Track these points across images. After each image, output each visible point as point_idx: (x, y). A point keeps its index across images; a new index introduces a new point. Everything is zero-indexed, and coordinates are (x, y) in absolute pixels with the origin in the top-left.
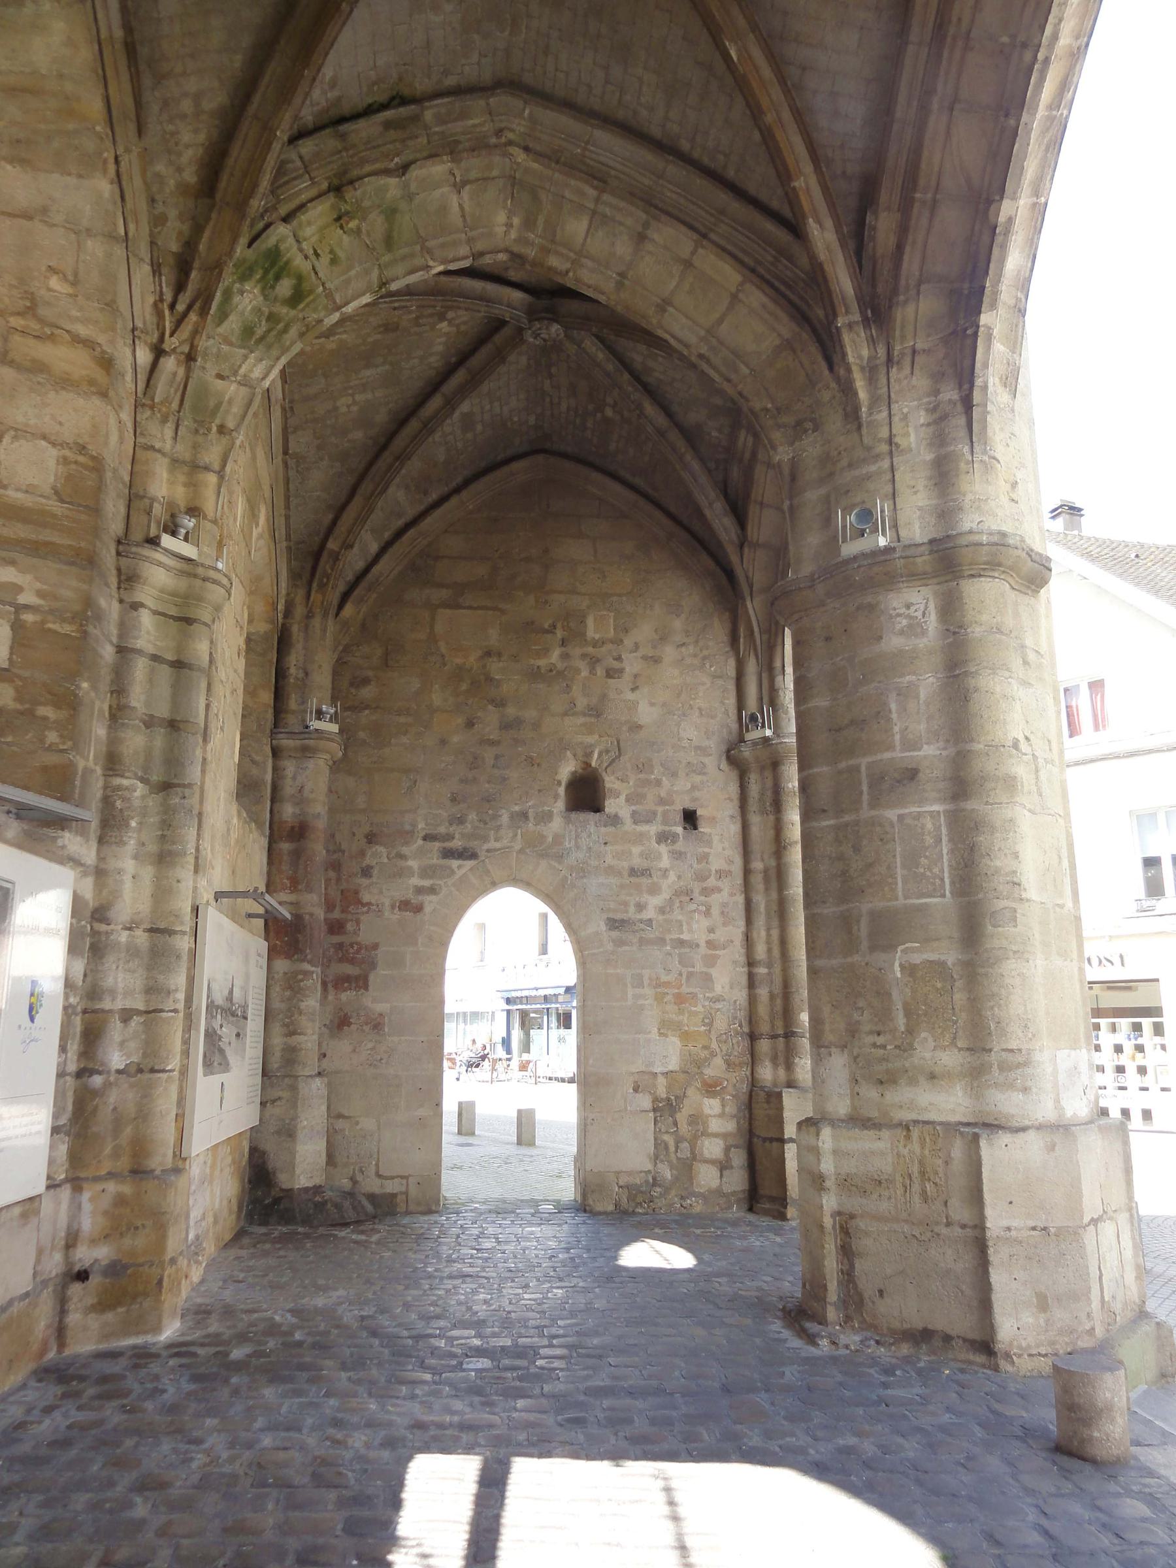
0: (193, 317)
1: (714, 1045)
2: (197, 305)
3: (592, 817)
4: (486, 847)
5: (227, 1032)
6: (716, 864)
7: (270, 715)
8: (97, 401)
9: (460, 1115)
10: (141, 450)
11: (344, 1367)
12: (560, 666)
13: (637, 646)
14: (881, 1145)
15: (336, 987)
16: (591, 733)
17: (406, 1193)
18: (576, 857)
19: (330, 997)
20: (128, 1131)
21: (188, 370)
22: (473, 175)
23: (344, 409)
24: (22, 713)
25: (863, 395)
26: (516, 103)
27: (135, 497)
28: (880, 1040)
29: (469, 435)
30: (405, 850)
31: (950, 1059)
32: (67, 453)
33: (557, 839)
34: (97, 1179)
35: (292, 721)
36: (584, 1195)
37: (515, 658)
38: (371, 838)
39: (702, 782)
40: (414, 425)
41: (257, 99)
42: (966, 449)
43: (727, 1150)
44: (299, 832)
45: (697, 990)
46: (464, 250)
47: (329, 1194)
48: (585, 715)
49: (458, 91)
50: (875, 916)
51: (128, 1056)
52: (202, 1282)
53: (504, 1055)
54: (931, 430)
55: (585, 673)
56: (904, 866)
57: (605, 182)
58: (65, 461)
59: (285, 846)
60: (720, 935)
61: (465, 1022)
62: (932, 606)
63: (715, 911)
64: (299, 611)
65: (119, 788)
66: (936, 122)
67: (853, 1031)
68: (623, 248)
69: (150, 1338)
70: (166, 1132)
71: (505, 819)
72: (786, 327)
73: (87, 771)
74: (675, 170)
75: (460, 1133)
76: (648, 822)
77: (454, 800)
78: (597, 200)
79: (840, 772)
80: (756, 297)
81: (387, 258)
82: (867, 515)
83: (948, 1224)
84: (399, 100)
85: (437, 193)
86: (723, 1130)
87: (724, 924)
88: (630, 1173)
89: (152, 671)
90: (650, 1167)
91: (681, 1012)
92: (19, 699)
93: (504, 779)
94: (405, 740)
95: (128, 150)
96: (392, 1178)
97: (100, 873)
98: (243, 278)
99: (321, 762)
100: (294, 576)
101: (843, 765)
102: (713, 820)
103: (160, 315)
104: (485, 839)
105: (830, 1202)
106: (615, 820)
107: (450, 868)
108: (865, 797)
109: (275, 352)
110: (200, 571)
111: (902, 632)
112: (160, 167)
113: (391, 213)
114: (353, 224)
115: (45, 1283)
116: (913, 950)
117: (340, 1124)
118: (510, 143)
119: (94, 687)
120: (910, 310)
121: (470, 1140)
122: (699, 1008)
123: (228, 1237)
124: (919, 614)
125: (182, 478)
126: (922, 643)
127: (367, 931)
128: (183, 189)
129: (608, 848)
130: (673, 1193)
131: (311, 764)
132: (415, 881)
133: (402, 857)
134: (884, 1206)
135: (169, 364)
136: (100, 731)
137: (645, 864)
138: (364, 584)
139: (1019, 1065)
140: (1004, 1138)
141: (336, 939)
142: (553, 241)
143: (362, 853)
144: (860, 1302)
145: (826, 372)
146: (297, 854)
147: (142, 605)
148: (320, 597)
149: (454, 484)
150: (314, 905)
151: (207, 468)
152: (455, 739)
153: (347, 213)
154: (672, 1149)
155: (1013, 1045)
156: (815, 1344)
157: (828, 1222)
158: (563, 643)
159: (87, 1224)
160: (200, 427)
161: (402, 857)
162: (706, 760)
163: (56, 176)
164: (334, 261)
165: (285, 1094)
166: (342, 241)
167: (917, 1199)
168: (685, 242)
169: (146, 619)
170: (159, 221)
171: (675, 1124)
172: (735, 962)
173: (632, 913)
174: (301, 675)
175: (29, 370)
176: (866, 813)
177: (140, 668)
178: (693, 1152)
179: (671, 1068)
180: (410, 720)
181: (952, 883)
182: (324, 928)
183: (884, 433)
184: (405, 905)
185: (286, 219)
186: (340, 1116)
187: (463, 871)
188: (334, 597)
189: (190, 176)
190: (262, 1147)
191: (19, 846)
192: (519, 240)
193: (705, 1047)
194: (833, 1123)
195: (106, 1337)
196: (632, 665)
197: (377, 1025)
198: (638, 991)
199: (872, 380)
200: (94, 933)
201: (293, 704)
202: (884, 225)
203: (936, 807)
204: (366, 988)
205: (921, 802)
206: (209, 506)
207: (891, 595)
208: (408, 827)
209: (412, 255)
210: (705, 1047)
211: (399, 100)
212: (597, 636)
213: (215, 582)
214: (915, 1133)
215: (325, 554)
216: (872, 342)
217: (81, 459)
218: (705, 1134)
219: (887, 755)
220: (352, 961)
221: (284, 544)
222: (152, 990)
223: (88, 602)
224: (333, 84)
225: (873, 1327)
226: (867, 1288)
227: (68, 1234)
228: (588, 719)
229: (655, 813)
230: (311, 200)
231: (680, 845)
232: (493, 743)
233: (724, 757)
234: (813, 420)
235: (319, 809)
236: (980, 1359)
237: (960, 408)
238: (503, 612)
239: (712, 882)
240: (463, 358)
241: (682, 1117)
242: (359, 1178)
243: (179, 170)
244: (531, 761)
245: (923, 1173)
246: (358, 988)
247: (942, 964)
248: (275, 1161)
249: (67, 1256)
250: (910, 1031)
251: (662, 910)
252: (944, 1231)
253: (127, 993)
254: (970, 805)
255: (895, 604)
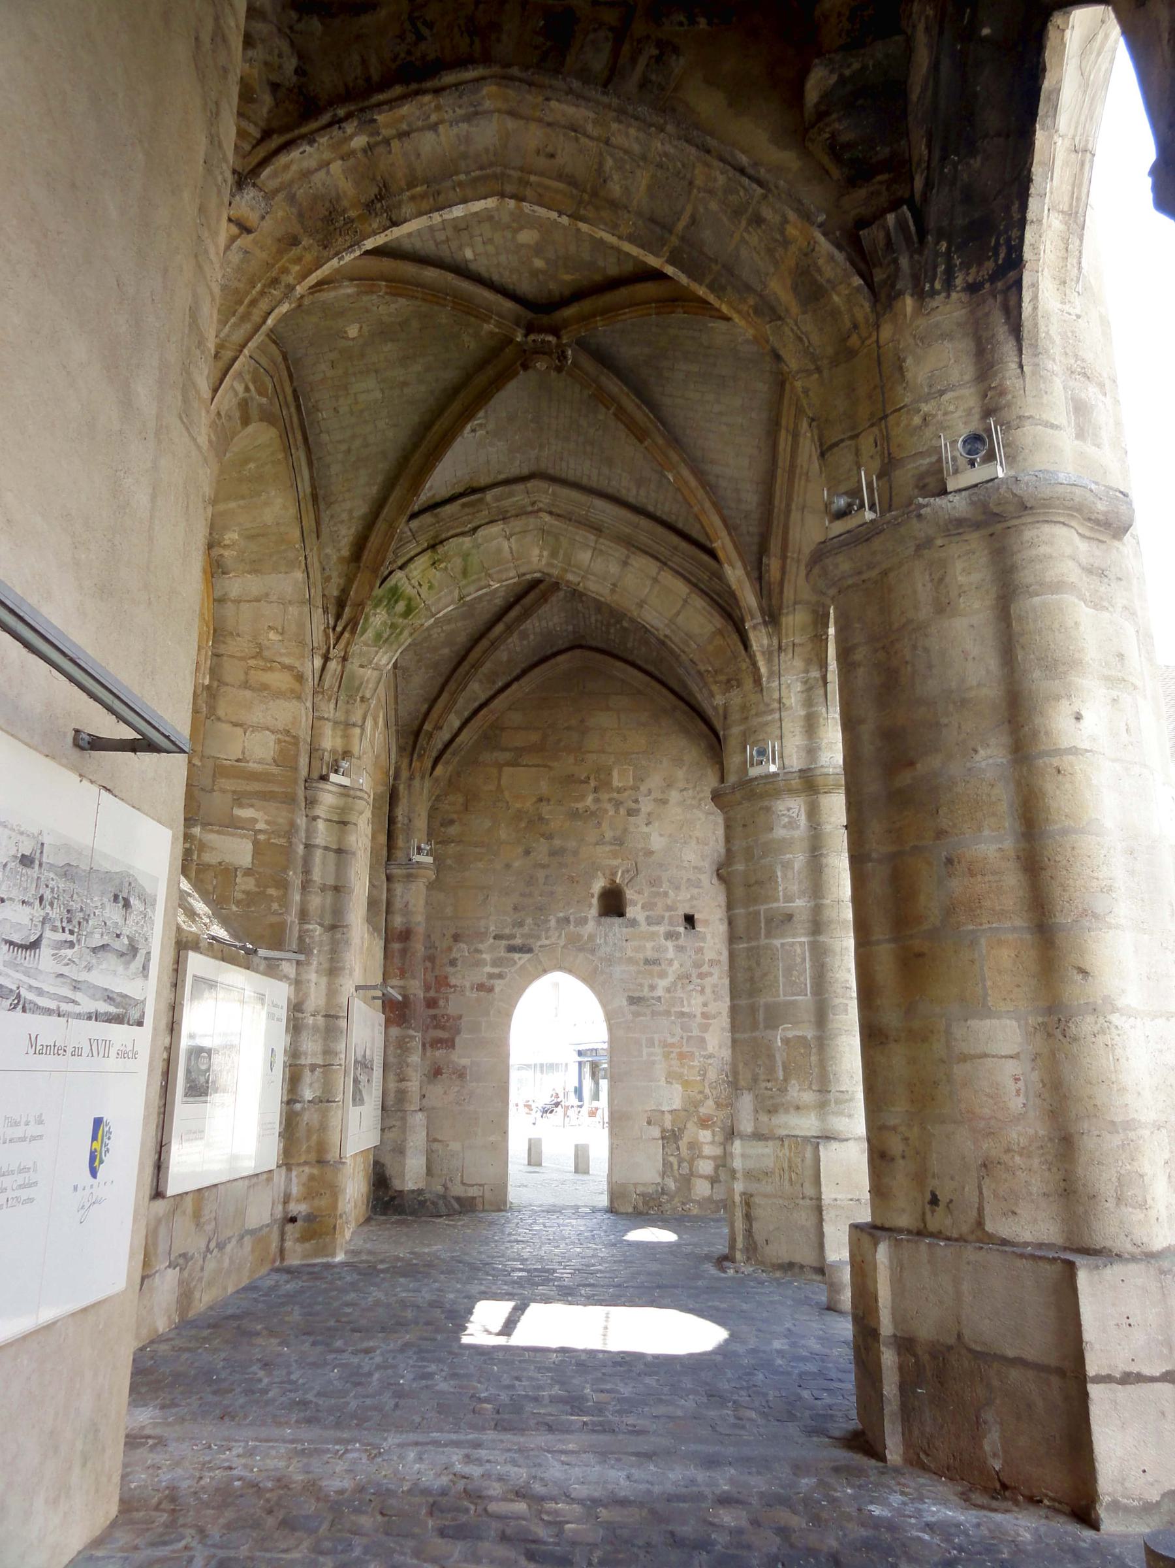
0: (346, 635)
1: (707, 1091)
2: (349, 628)
3: (617, 921)
4: (539, 943)
5: (363, 1078)
6: (709, 955)
7: (385, 852)
8: (295, 702)
9: (530, 1149)
10: (317, 719)
11: (442, 1273)
12: (593, 808)
13: (650, 792)
14: (767, 1151)
15: (431, 1046)
16: (616, 857)
17: (483, 1197)
18: (604, 950)
19: (428, 1054)
20: (314, 1138)
21: (343, 667)
22: (518, 529)
23: (436, 636)
24: (259, 893)
25: (763, 670)
26: (543, 485)
27: (314, 750)
28: (769, 1085)
29: (525, 642)
30: (481, 946)
31: (808, 1097)
32: (280, 736)
33: (591, 938)
34: (299, 1165)
35: (400, 855)
36: (611, 1200)
37: (560, 802)
38: (456, 938)
39: (699, 894)
40: (485, 643)
41: (385, 511)
42: (824, 710)
43: (717, 1168)
44: (406, 935)
45: (694, 1049)
46: (512, 573)
47: (428, 1196)
48: (611, 844)
49: (507, 482)
50: (767, 1007)
51: (314, 1092)
52: (351, 1240)
53: (576, 1102)
54: (804, 695)
55: (611, 813)
56: (784, 976)
57: (601, 531)
58: (279, 741)
59: (396, 946)
60: (713, 1008)
61: (542, 1072)
62: (803, 810)
63: (708, 990)
64: (405, 774)
65: (308, 930)
66: (795, 516)
67: (755, 1080)
68: (614, 568)
69: (329, 1259)
70: (334, 1138)
71: (553, 923)
72: (718, 622)
73: (293, 922)
74: (644, 522)
75: (529, 1164)
76: (658, 923)
77: (515, 909)
78: (596, 542)
79: (750, 914)
80: (699, 602)
81: (464, 582)
82: (763, 752)
83: (803, 1198)
84: (474, 491)
85: (495, 542)
86: (713, 1154)
87: (715, 1000)
88: (644, 1185)
89: (324, 857)
90: (659, 1180)
91: (682, 1065)
92: (258, 886)
93: (552, 893)
94: (480, 865)
95: (311, 550)
96: (472, 1186)
97: (298, 983)
98: (376, 606)
99: (421, 885)
100: (401, 749)
101: (751, 909)
102: (706, 922)
103: (327, 637)
104: (539, 938)
105: (739, 1187)
106: (633, 923)
107: (513, 959)
108: (763, 931)
109: (394, 647)
110: (352, 792)
111: (784, 826)
112: (328, 551)
113: (466, 556)
114: (442, 566)
115: (275, 1220)
116: (788, 1029)
117: (435, 1146)
118: (540, 510)
119: (295, 873)
120: (791, 618)
121: (537, 1169)
122: (696, 1063)
123: (362, 1220)
124: (795, 815)
125: (339, 733)
126: (797, 834)
127: (452, 1006)
128: (341, 560)
129: (629, 944)
130: (676, 1200)
131: (413, 886)
132: (488, 969)
133: (478, 951)
134: (769, 1189)
135: (333, 665)
136: (297, 897)
137: (656, 956)
138: (450, 750)
139: (847, 1101)
140: (834, 1145)
141: (432, 1012)
142: (569, 565)
143: (450, 949)
144: (755, 1249)
145: (743, 652)
146: (404, 952)
147: (318, 817)
148: (418, 764)
149: (514, 674)
150: (416, 989)
151: (354, 725)
152: (517, 864)
153: (439, 560)
154: (676, 1167)
155: (843, 1089)
156: (725, 1272)
157: (737, 1199)
158: (596, 790)
159: (295, 1190)
160: (350, 700)
161: (478, 951)
162: (703, 877)
163: (273, 575)
164: (430, 588)
165: (398, 1123)
166: (436, 575)
167: (786, 1183)
168: (652, 567)
169: (321, 825)
170: (328, 579)
171: (678, 1149)
172: (723, 1029)
173: (646, 992)
174: (406, 821)
175: (259, 690)
176: (763, 941)
177: (318, 854)
178: (691, 1170)
179: (674, 1107)
180: (483, 850)
181: (812, 987)
182: (423, 1003)
183: (776, 696)
184: (481, 987)
185: (401, 568)
186: (435, 1140)
187: (522, 962)
188: (428, 764)
189: (346, 553)
190: (382, 1160)
191: (265, 974)
192: (549, 565)
193: (701, 1092)
194: (742, 1137)
195: (305, 1257)
196: (646, 806)
197: (461, 1074)
198: (652, 1050)
199: (769, 661)
200: (295, 1019)
201: (400, 843)
202: (773, 565)
203: (803, 939)
204: (453, 1047)
205: (794, 936)
206: (356, 750)
207: (779, 802)
208: (483, 930)
209: (479, 579)
210: (701, 1092)
211: (474, 491)
212: (620, 785)
213: (361, 798)
214: (786, 1143)
215: (422, 735)
216: (770, 636)
217: (287, 739)
218: (700, 1156)
219: (775, 905)
220: (443, 1028)
221: (394, 728)
222: (328, 1052)
223: (292, 824)
224: (431, 488)
225: (763, 1263)
226: (759, 1238)
227: (285, 1195)
228: (613, 847)
229: (663, 917)
230: (416, 555)
231: (682, 941)
232: (543, 866)
233: (715, 875)
234: (737, 680)
235: (419, 919)
236: (818, 1278)
237: (821, 683)
238: (550, 768)
239: (705, 968)
240: (519, 599)
241: (683, 1144)
242: (449, 1184)
243: (339, 550)
244: (572, 880)
245: (790, 1167)
246: (447, 1047)
247: (804, 1038)
248: (391, 1171)
249: (284, 1208)
250: (786, 1080)
251: (668, 990)
252: (801, 1202)
253: (314, 1054)
254: (822, 938)
255: (781, 808)
